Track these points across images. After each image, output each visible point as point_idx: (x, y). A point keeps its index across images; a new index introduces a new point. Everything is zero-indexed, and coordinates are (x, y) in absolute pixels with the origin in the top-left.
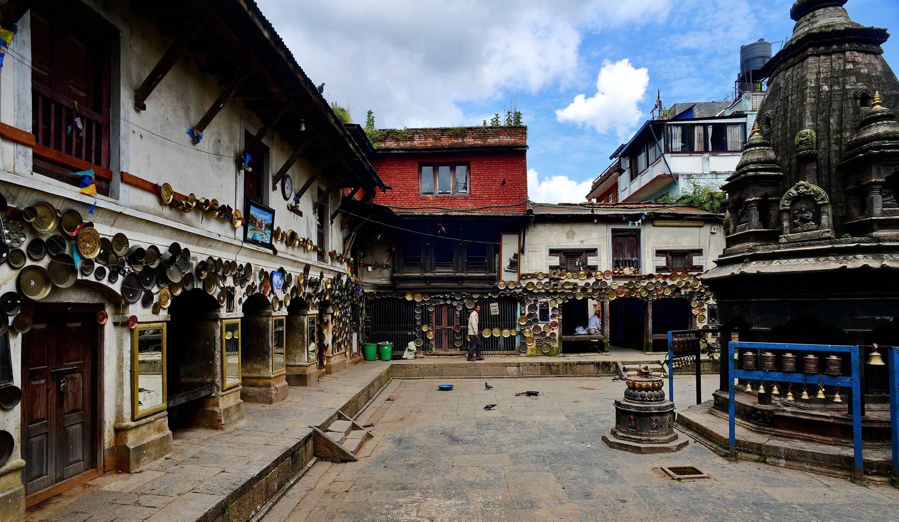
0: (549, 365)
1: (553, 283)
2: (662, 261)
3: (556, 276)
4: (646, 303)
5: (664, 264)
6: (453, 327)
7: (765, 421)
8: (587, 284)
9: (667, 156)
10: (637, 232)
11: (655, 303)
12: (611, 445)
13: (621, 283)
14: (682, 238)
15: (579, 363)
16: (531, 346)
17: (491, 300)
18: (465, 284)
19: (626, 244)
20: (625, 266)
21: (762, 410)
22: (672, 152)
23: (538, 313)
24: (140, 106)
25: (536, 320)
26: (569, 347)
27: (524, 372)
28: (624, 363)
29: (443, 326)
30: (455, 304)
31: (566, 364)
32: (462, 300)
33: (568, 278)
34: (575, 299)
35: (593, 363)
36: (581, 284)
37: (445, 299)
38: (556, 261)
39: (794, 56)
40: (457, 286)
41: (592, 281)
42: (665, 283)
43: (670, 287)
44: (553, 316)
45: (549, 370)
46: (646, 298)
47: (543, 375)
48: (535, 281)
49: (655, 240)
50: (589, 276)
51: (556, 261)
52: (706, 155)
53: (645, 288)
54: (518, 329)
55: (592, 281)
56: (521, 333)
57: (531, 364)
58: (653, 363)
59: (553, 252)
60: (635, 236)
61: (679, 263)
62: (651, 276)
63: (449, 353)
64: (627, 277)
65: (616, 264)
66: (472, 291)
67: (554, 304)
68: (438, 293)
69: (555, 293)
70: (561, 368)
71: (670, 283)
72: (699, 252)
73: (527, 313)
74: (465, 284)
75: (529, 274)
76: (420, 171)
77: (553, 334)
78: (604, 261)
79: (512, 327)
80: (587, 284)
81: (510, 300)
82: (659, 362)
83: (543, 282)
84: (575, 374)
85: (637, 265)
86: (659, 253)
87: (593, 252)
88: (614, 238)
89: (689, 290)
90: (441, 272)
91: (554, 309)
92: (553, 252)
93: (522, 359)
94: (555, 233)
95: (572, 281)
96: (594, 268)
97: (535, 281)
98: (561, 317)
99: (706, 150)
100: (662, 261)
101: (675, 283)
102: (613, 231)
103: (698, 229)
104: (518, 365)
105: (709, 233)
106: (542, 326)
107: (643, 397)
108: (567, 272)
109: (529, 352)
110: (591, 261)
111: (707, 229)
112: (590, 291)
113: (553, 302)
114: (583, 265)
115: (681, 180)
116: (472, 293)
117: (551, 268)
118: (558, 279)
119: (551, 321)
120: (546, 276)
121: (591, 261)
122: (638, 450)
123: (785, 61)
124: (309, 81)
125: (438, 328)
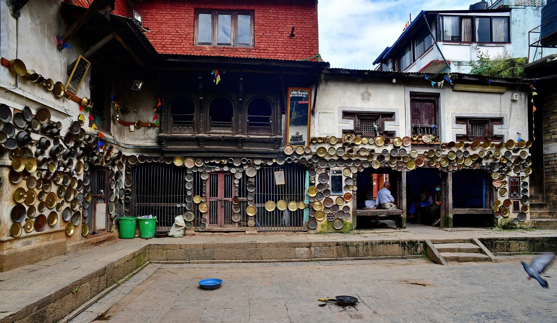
0: (346, 245)
1: (347, 149)
2: (462, 130)
3: (350, 142)
4: (445, 175)
5: (352, 128)
6: (230, 199)
8: (385, 151)
9: (440, 44)
10: (437, 96)
11: (455, 175)
13: (421, 151)
14: (484, 105)
15: (382, 243)
16: (322, 221)
17: (276, 167)
18: (246, 148)
19: (425, 109)
20: (424, 134)
22: (444, 41)
23: (329, 183)
25: (327, 191)
26: (365, 223)
27: (316, 254)
28: (434, 242)
29: (219, 198)
30: (233, 171)
31: (367, 244)
32: (242, 166)
33: (364, 144)
35: (398, 242)
36: (379, 151)
37: (221, 165)
38: (350, 125)
40: (236, 149)
41: (390, 148)
42: (467, 152)
43: (471, 157)
44: (347, 187)
45: (346, 252)
46: (447, 168)
47: (339, 258)
48: (327, 147)
49: (454, 106)
50: (387, 142)
51: (350, 125)
52: (474, 45)
53: (446, 158)
54: (306, 202)
55: (390, 148)
56: (310, 207)
57: (325, 244)
58: (464, 241)
59: (347, 114)
60: (434, 102)
61: (478, 132)
62: (452, 144)
64: (425, 145)
65: (415, 131)
66: (254, 155)
67: (348, 173)
68: (214, 158)
69: (350, 161)
70: (360, 248)
71: (472, 153)
72: (499, 121)
73: (317, 183)
74: (246, 148)
75: (320, 138)
76: (196, 18)
77: (347, 208)
78: (402, 127)
79: (300, 198)
80: (385, 151)
81: (297, 169)
82: (472, 241)
83: (336, 147)
84: (377, 257)
85: (435, 131)
86: (460, 120)
87: (390, 116)
88: (412, 101)
89: (490, 161)
91: (348, 178)
92: (347, 114)
93: (312, 238)
94: (349, 93)
95: (367, 147)
96: (391, 134)
97: (327, 147)
98: (355, 188)
99: (473, 40)
100: (462, 130)
101: (477, 152)
102: (412, 94)
103: (498, 97)
104: (309, 246)
105: (508, 102)
106: (334, 198)
108: (362, 137)
109: (319, 229)
110: (389, 126)
111: (507, 96)
112: (387, 159)
113: (347, 171)
114: (379, 130)
115: (452, 66)
116: (253, 159)
117: (345, 132)
118: (353, 145)
119: (344, 192)
120: (340, 141)
121: (389, 126)
125: (213, 199)
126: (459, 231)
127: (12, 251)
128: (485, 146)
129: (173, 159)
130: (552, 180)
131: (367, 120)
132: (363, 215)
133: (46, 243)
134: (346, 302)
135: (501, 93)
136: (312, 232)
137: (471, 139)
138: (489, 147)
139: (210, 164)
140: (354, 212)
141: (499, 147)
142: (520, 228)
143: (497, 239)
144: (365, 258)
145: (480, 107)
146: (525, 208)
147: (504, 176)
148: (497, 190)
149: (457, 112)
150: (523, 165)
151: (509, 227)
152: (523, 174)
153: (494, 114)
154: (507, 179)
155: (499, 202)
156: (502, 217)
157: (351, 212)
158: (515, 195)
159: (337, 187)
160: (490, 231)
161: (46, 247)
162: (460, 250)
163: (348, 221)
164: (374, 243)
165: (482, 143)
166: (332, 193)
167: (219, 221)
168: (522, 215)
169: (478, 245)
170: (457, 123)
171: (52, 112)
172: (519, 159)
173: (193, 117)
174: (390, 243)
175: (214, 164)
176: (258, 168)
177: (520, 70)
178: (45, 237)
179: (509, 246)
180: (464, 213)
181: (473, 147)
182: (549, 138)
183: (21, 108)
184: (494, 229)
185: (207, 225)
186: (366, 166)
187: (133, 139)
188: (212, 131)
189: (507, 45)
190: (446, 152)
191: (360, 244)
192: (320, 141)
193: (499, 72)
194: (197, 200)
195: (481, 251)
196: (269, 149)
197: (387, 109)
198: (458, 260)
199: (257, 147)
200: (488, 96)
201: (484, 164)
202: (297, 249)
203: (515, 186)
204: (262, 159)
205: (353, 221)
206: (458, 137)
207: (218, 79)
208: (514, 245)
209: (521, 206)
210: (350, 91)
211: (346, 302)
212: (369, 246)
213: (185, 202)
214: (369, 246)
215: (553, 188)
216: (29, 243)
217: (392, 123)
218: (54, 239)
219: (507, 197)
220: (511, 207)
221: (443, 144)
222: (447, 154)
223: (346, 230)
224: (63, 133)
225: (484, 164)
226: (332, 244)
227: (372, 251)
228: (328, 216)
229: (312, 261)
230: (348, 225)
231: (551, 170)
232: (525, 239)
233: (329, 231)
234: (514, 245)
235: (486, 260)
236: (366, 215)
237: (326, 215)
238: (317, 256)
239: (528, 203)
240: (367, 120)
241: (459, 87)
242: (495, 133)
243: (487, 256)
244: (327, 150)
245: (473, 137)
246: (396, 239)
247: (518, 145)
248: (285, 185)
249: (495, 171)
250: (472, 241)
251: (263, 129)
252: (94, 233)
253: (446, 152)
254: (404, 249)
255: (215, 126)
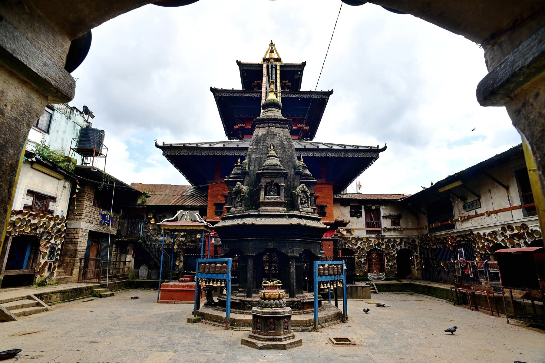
2: (29, 201)
5: (30, 204)
7: (298, 308)
12: (253, 345)
21: (297, 302)
39: (279, 124)
43: (32, 225)
58: (23, 298)
61: (39, 206)
62: (20, 212)
71: (33, 222)
72: (54, 199)
78: (60, 208)
82: (29, 298)
86: (30, 193)
89: (42, 230)
100: (29, 201)
103: (57, 181)
105: (62, 187)
107: (276, 304)
122: (283, 347)
123: (275, 123)
126: (6, 291)
128: (42, 217)
130: (69, 248)
135: (59, 180)
137: (34, 210)
138: (44, 219)
141: (50, 219)
142: (49, 284)
143: (45, 294)
145: (45, 186)
146: (55, 267)
147: (48, 242)
148: (41, 253)
149: (30, 186)
150: (60, 235)
151: (42, 284)
152: (58, 242)
153: (52, 194)
154: (49, 245)
155: (41, 263)
156: (39, 276)
158: (51, 258)
160: (30, 289)
162: (22, 306)
165: (41, 215)
168: (52, 274)
169: (35, 300)
170: (27, 195)
172: (59, 230)
177: (72, 167)
179: (50, 299)
180: (13, 274)
181: (34, 217)
182: (73, 217)
184: (32, 287)
189: (46, 135)
190: (14, 218)
193: (57, 162)
195: (38, 304)
198: (24, 314)
200: (52, 178)
201: (38, 232)
203: (53, 249)
206: (26, 207)
208: (54, 296)
209: (53, 266)
215: (68, 253)
217: (54, 203)
219: (46, 260)
220: (47, 267)
221: (13, 210)
222: (14, 220)
225: (38, 232)
231: (70, 240)
232: (60, 292)
234: (54, 296)
235: (44, 310)
239: (57, 264)
241: (35, 166)
242: (50, 208)
243: (43, 308)
245: (35, 208)
247: (61, 220)
249: (43, 238)
250: (29, 298)
253: (14, 218)
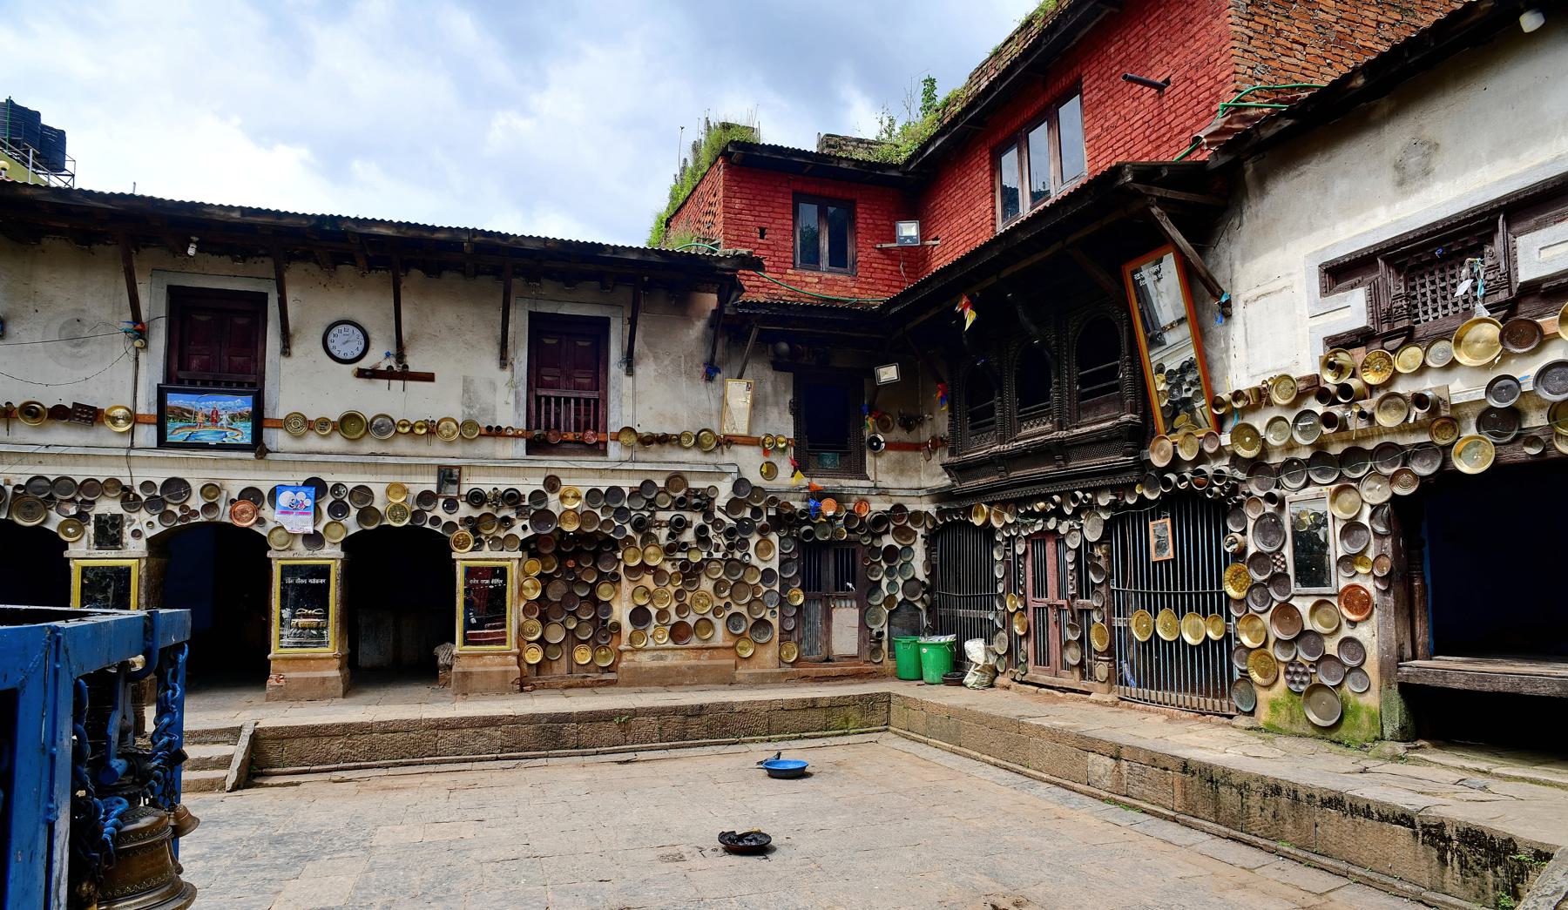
15: (1334, 802)
18: (1076, 465)
24: (630, 371)
34: (1448, 477)
35: (1405, 819)
38: (1352, 309)
47: (1184, 817)
51: (1352, 309)
59: (1338, 274)
63: (1058, 682)
70: (1255, 801)
74: (1076, 465)
90: (1038, 431)
106: (1303, 606)
109: (1264, 715)
112: (1536, 420)
117: (1339, 343)
124: (798, 153)
127: (632, 665)
129: (968, 511)
131: (1433, 261)
132: (1429, 681)
133: (693, 662)
134: (747, 845)
136: (1241, 721)
139: (1032, 514)
140: (1388, 669)
144: (1262, 842)
157: (1372, 667)
159: (1312, 567)
161: (690, 668)
163: (1362, 700)
164: (1301, 795)
166: (1295, 588)
167: (1052, 659)
171: (687, 476)
173: (992, 408)
174: (1368, 815)
175: (1032, 514)
176: (1105, 516)
178: (692, 654)
183: (638, 484)
185: (1030, 666)
186: (1423, 469)
187: (901, 482)
188: (1024, 432)
191: (1254, 785)
192: (1239, 405)
194: (1012, 604)
196: (1111, 458)
197: (1530, 170)
199: (1095, 457)
202: (1091, 756)
204: (1113, 489)
205: (1385, 701)
207: (970, 317)
210: (1345, 174)
211: (747, 845)
212: (1284, 800)
213: (994, 608)
214: (1284, 800)
216: (662, 658)
218: (710, 658)
223: (1360, 736)
224: (722, 500)
226: (1171, 764)
227: (1297, 825)
228: (1287, 672)
229: (1116, 802)
230: (1364, 717)
233: (1294, 729)
236: (1439, 683)
237: (1282, 669)
238: (1134, 791)
240: (1433, 261)
244: (1262, 432)
246: (1401, 798)
248: (1174, 561)
251: (1106, 401)
252: (828, 660)
254: (1443, 860)
255: (1027, 419)
